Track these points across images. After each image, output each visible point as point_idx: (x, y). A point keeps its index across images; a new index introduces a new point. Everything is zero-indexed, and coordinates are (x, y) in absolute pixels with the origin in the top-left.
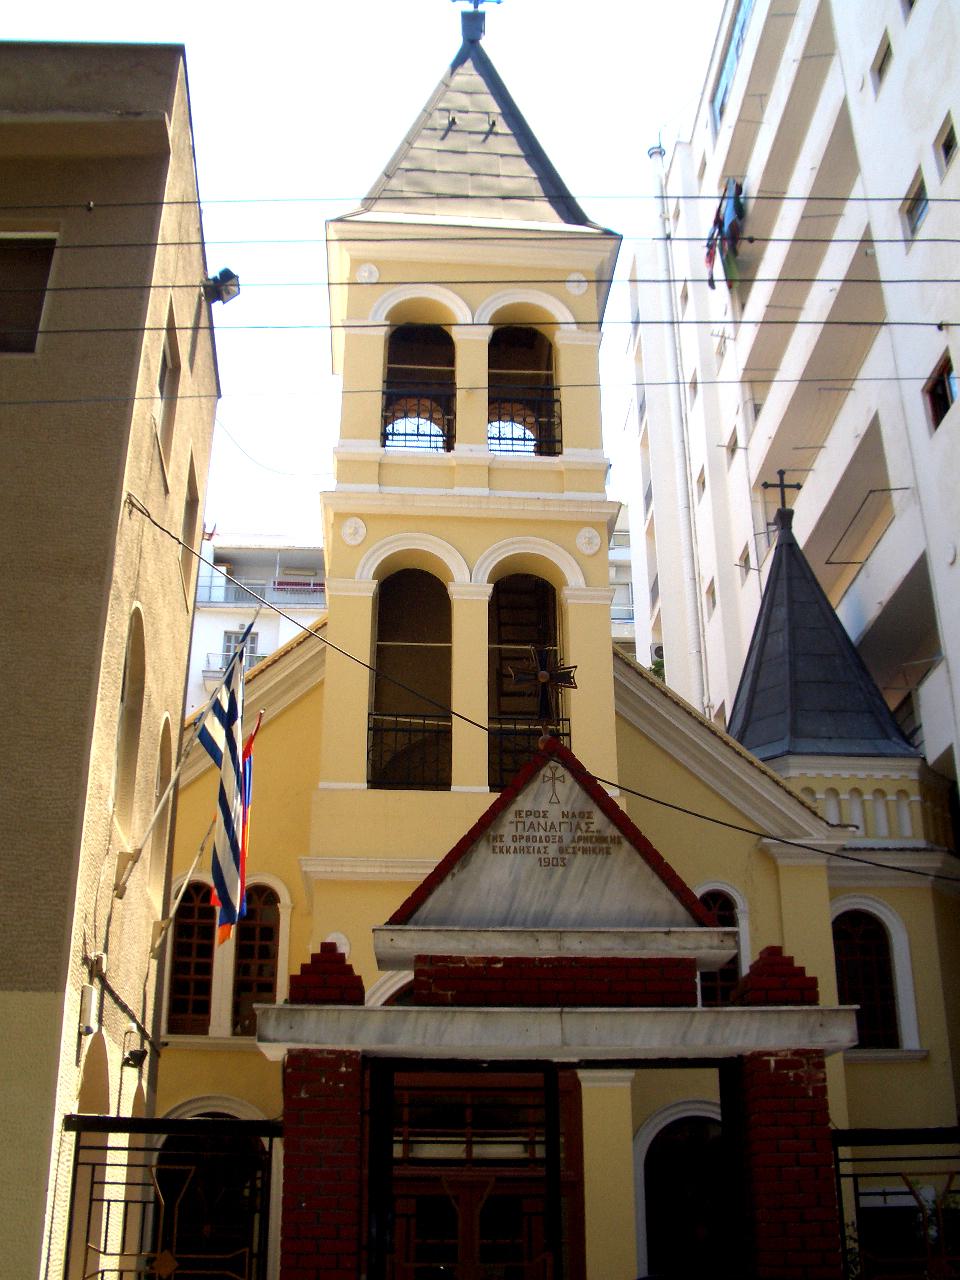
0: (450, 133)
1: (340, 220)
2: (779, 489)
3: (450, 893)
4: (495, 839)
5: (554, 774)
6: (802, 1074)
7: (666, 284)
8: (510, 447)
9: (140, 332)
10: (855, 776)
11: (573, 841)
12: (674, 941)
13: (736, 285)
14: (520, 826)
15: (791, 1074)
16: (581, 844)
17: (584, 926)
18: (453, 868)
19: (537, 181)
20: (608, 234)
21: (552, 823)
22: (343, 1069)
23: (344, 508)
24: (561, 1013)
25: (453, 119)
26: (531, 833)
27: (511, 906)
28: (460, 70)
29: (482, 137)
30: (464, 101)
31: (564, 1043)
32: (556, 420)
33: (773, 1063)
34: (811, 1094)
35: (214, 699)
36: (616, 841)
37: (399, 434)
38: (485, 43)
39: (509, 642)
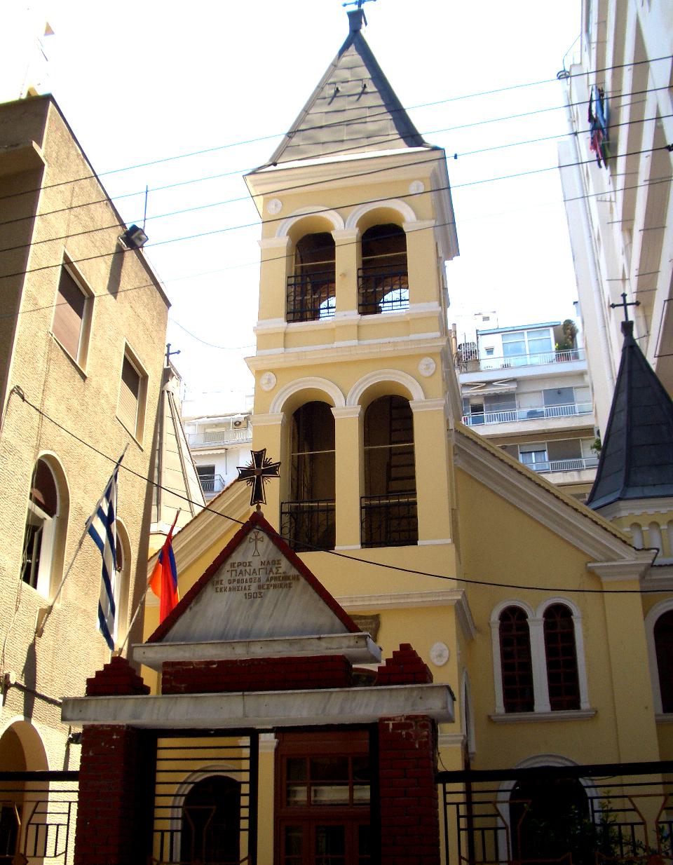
0: (335, 99)
1: (253, 173)
2: (623, 307)
3: (189, 620)
4: (217, 582)
5: (256, 537)
6: (412, 733)
7: (577, 166)
8: (399, 307)
9: (289, 254)
10: (633, 514)
11: (267, 580)
12: (323, 644)
13: (609, 160)
14: (234, 573)
15: (404, 733)
16: (273, 582)
17: (271, 639)
18: (190, 604)
19: (392, 121)
20: (435, 149)
21: (255, 569)
22: (115, 737)
23: (261, 367)
24: (243, 695)
25: (337, 89)
26: (240, 577)
27: (226, 627)
28: (346, 53)
29: (357, 97)
30: (346, 74)
31: (245, 715)
32: (361, 291)
33: (391, 726)
34: (417, 746)
35: (98, 506)
36: (296, 578)
37: (405, 300)
38: (365, 32)
39: (397, 443)
